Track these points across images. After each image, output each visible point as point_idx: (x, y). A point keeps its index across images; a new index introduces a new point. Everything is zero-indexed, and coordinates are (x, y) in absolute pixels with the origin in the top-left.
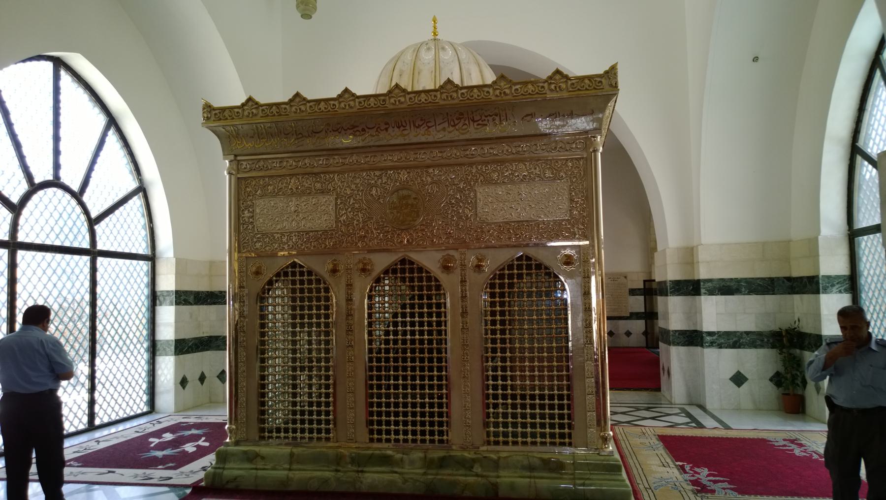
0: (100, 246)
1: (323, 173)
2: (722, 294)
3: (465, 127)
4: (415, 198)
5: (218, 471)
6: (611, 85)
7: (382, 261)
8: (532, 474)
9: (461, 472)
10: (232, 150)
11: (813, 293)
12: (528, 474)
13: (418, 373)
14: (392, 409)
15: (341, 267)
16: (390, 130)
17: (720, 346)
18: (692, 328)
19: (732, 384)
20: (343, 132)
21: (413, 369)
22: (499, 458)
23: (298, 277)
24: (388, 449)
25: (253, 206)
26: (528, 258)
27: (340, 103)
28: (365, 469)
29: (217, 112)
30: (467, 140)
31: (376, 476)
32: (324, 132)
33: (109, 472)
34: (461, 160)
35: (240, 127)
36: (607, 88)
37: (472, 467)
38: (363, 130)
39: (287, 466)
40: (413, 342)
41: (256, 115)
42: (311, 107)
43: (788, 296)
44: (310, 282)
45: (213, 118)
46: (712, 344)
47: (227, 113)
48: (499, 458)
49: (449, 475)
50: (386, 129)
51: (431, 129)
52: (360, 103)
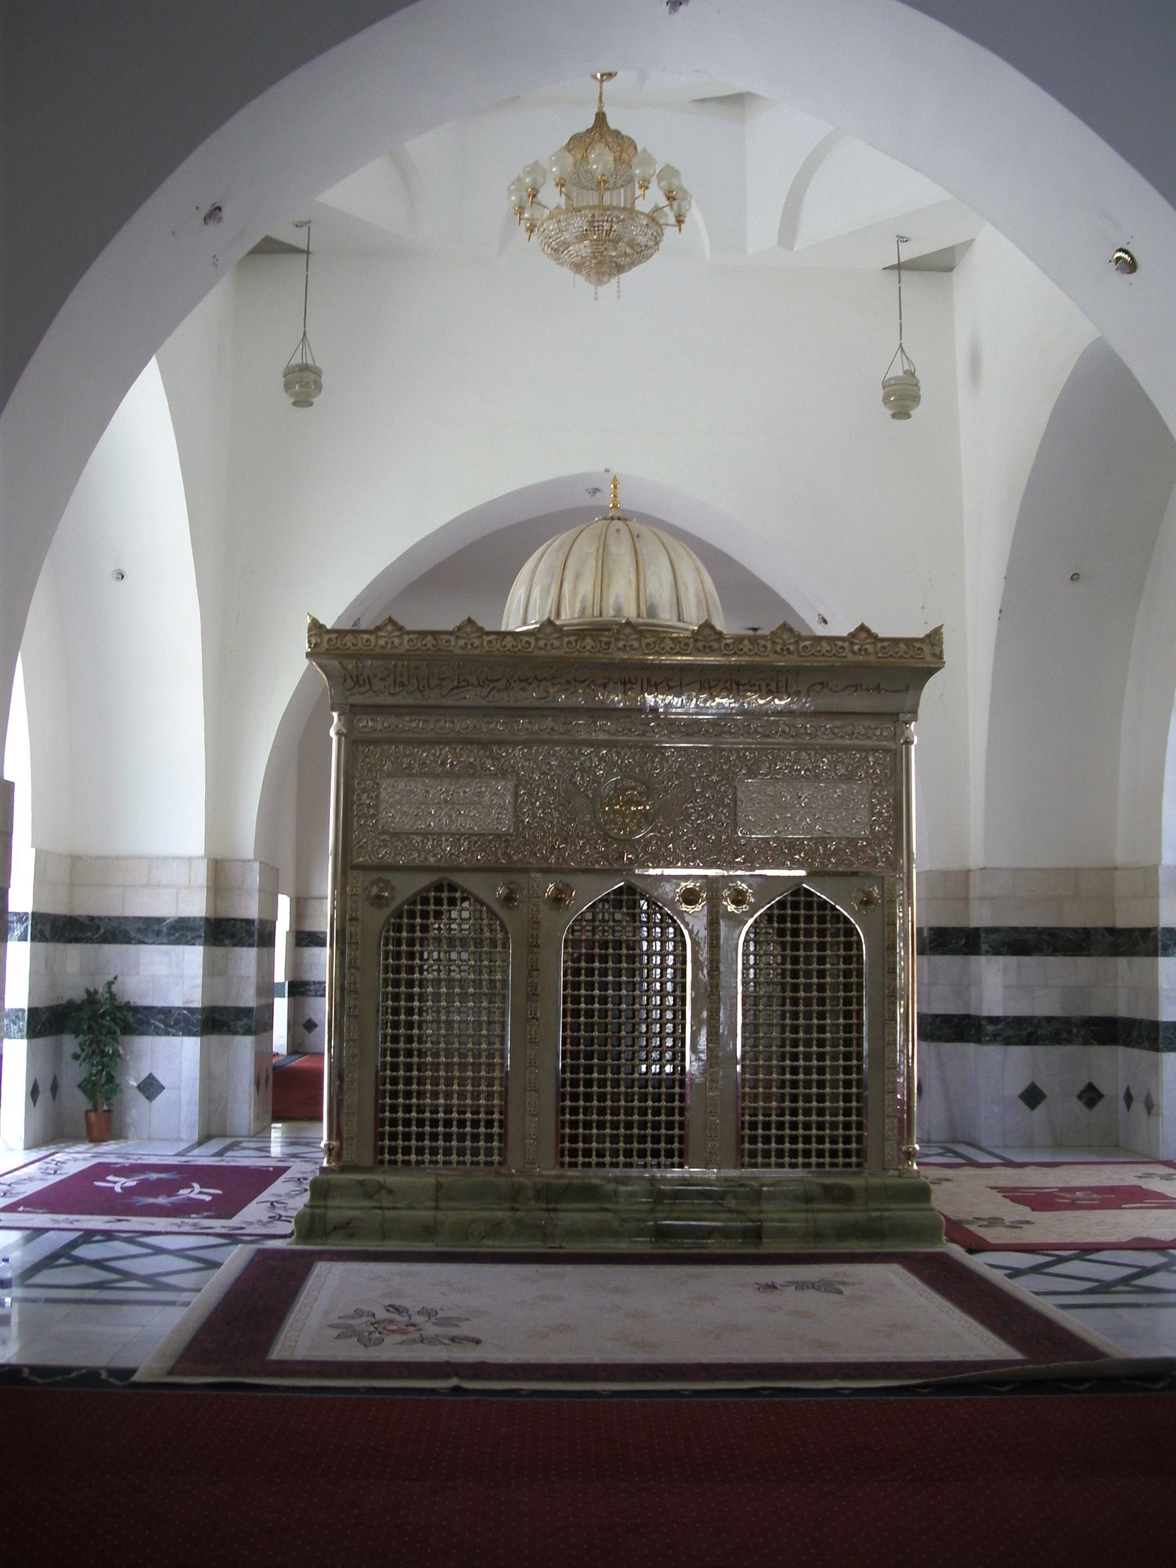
2: (1014, 953)
5: (317, 1211)
6: (934, 655)
11: (1147, 955)
12: (803, 1206)
17: (1008, 1042)
18: (962, 1011)
19: (1021, 1104)
20: (535, 683)
24: (594, 1176)
27: (377, 637)
28: (559, 1206)
31: (577, 1216)
33: (119, 1220)
36: (928, 658)
42: (490, 642)
43: (1110, 960)
46: (995, 1039)
49: (689, 1211)
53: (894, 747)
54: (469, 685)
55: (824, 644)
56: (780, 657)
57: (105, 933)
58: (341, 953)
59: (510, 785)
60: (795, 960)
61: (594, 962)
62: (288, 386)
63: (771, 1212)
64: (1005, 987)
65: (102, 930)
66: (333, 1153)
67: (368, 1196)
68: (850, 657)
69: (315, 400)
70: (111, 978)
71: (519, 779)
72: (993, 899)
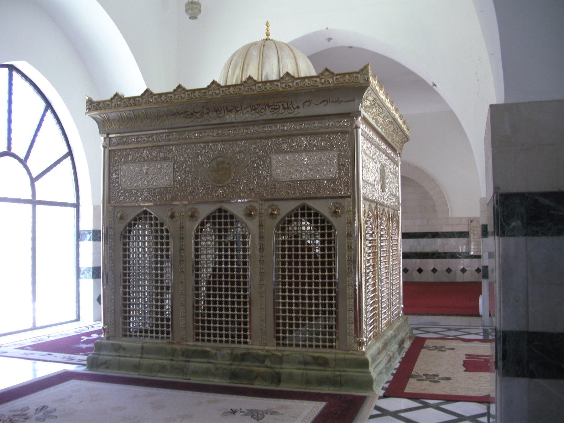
0: (38, 198)
1: (165, 146)
3: (263, 110)
4: (228, 164)
6: (365, 80)
7: (205, 210)
8: (306, 367)
9: (257, 364)
12: (303, 367)
13: (230, 292)
14: (212, 318)
15: (177, 215)
16: (210, 114)
21: (227, 290)
22: (283, 355)
24: (207, 347)
27: (175, 95)
29: (156, 97)
30: (265, 120)
31: (197, 365)
32: (165, 117)
34: (261, 135)
37: (264, 361)
39: (140, 355)
40: (226, 270)
41: (120, 106)
42: (155, 99)
45: (92, 109)
47: (101, 105)
48: (283, 355)
49: (248, 366)
50: (208, 113)
51: (239, 113)
52: (188, 95)
58: (106, 243)
59: (171, 164)
63: (286, 368)
66: (106, 330)
67: (116, 350)
71: (174, 161)
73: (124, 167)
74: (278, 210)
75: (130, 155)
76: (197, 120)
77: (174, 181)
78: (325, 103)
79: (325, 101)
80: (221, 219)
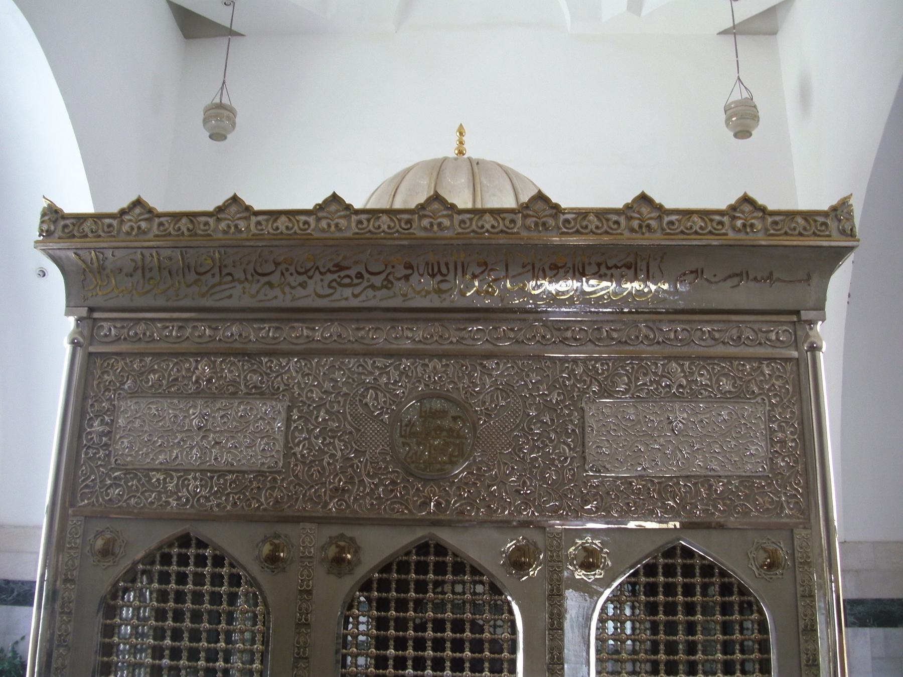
10: (85, 299)
16: (414, 279)
23: (191, 568)
25: (112, 410)
26: (441, 549)
27: (319, 220)
29: (68, 222)
35: (109, 253)
38: (360, 276)
41: (144, 233)
44: (217, 580)
47: (87, 226)
50: (407, 278)
53: (795, 354)
54: (233, 280)
55: (695, 218)
56: (638, 236)
57: (18, 595)
59: (281, 407)
60: (671, 648)
61: (387, 648)
62: (206, 121)
64: (873, 658)
65: (16, 593)
68: (731, 235)
69: (229, 136)
70: (18, 638)
71: (293, 399)
72: (857, 571)
73: (131, 404)
74: (357, 551)
75: (154, 371)
76: (370, 293)
77: (288, 452)
78: (735, 280)
79: (737, 275)
80: (170, 564)
